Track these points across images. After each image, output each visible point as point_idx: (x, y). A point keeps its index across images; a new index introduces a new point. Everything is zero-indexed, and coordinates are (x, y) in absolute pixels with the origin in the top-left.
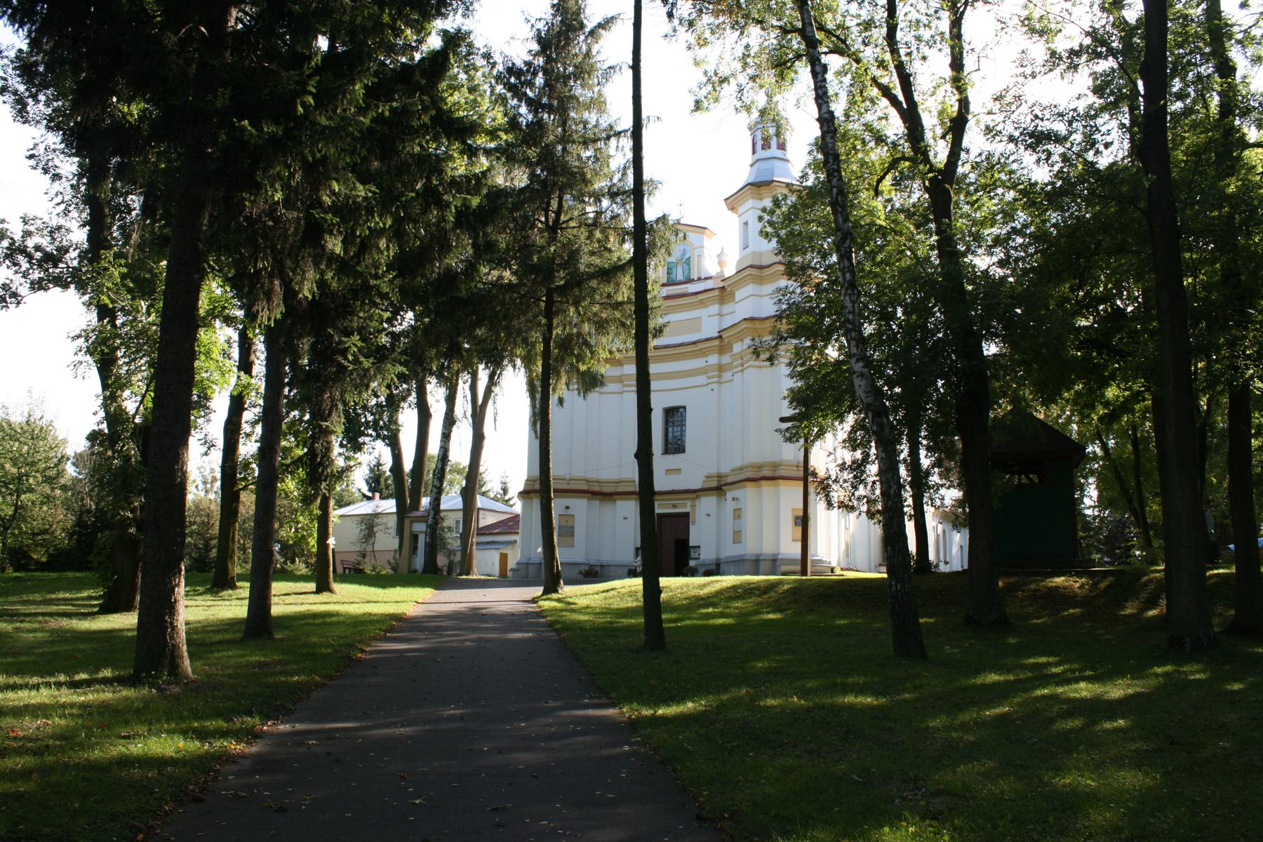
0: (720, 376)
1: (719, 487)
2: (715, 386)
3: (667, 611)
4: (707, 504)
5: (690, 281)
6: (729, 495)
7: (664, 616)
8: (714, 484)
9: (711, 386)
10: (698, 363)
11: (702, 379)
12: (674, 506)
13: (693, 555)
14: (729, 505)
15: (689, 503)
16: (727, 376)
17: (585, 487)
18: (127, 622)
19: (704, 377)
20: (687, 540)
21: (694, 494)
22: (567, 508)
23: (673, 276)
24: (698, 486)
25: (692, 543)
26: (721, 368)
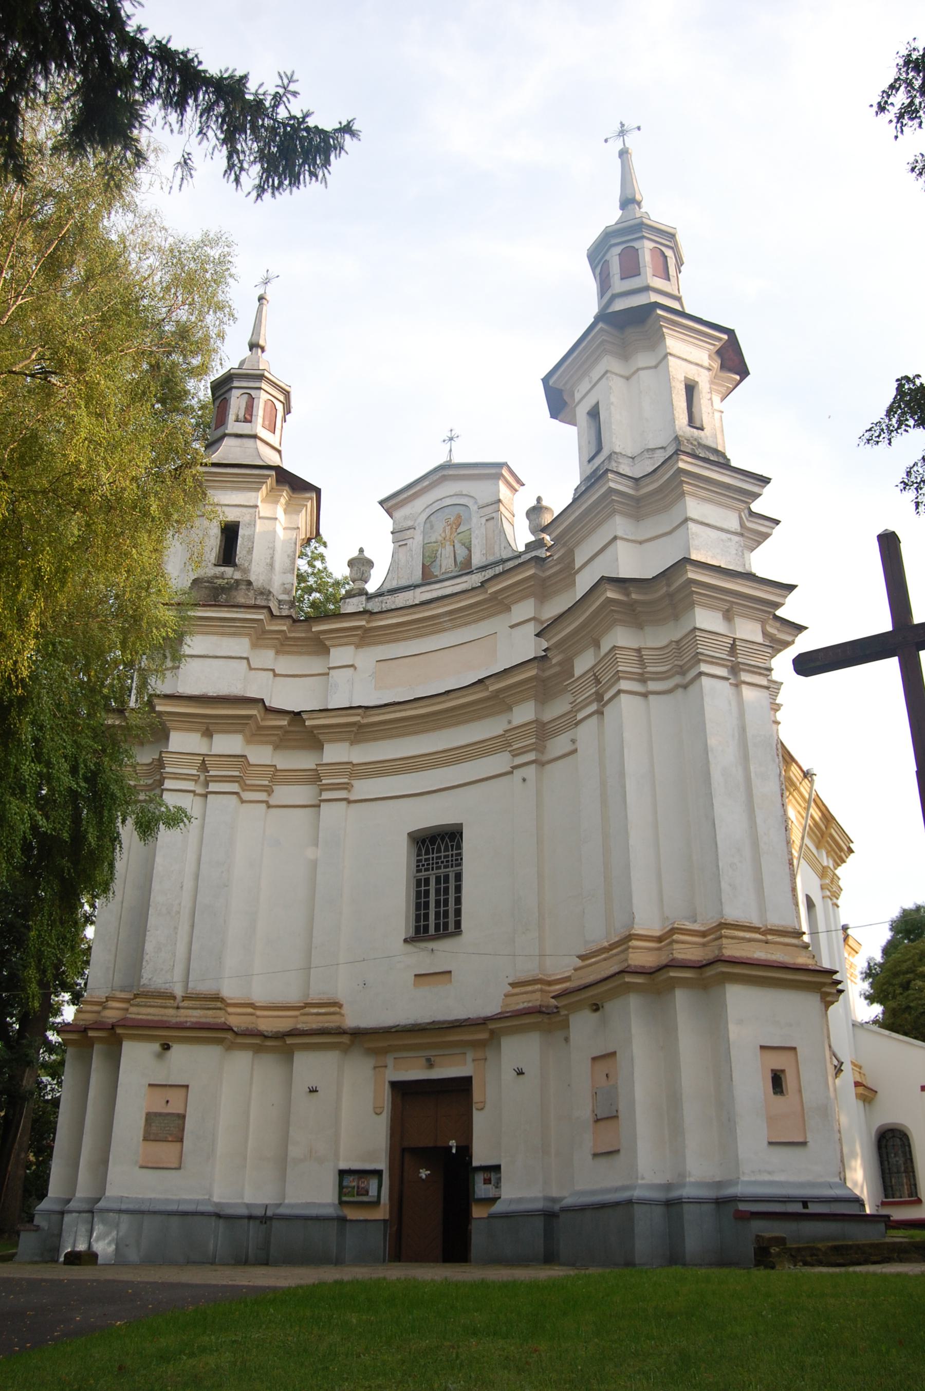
1: (546, 1011)
9: (519, 774)
11: (499, 762)
13: (481, 1189)
16: (559, 745)
21: (483, 1032)
24: (491, 1007)
26: (542, 732)
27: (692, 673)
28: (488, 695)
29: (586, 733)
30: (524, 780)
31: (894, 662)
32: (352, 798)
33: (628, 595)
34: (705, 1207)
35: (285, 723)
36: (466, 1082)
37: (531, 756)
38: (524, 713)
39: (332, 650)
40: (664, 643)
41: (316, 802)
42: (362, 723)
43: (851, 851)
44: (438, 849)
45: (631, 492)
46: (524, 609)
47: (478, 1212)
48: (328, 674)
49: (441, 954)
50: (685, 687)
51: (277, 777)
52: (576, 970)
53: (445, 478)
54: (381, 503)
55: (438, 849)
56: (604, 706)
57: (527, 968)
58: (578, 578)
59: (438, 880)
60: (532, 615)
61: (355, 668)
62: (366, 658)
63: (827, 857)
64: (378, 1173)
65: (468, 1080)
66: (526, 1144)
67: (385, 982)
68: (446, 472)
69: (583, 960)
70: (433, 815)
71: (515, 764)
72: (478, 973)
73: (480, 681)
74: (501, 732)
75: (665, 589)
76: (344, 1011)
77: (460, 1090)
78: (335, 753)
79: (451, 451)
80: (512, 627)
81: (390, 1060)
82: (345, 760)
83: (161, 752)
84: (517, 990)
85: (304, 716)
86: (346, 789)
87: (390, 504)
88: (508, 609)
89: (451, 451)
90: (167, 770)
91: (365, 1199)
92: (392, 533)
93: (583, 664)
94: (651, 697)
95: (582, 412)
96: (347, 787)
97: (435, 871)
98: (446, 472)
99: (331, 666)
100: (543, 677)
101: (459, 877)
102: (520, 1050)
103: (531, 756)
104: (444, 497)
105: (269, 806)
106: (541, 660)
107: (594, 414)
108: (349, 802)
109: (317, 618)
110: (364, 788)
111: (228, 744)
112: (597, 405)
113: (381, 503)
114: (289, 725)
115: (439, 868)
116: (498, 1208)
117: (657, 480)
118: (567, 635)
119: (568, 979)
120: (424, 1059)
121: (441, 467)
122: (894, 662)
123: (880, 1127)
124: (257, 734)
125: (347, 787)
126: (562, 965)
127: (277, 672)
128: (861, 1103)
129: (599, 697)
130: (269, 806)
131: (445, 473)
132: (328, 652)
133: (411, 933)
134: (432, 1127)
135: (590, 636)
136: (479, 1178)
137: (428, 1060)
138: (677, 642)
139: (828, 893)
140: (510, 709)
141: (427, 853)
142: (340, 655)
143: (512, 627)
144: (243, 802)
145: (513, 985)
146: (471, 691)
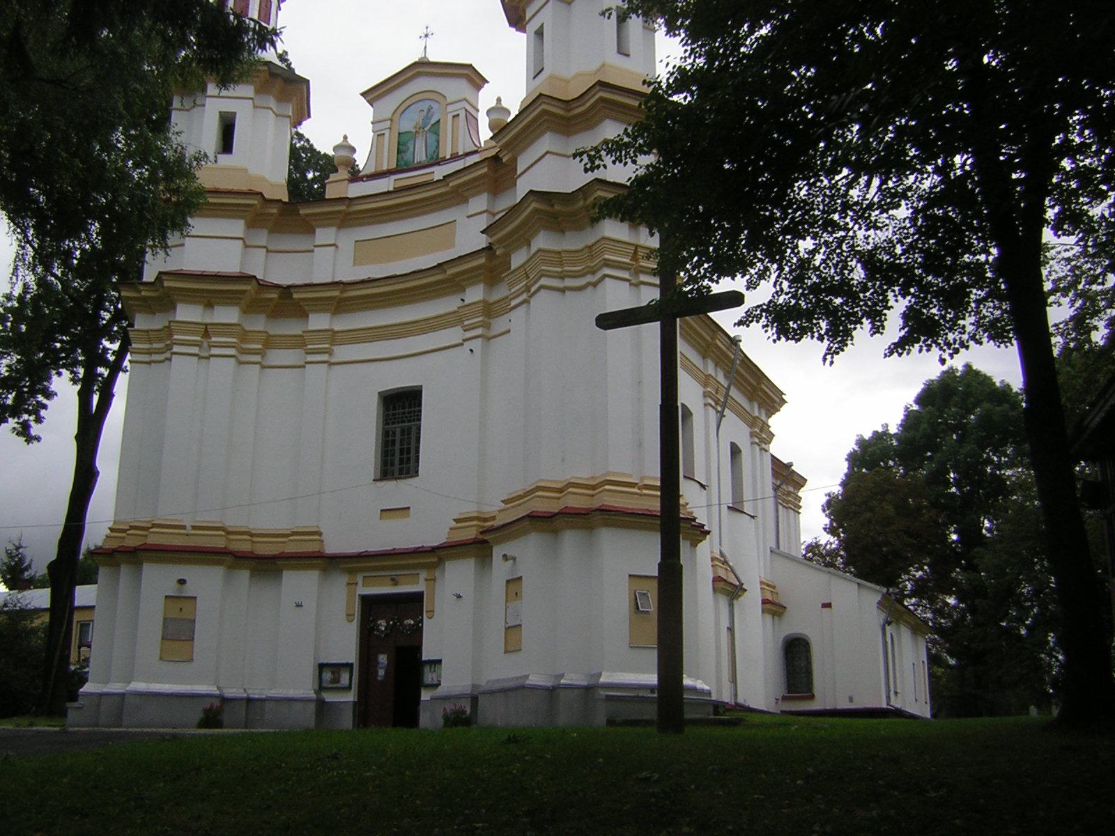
0: (487, 326)
1: (479, 543)
2: (477, 345)
3: (656, 496)
4: (458, 576)
5: (439, 162)
6: (498, 552)
7: (659, 493)
8: (470, 534)
9: (468, 345)
10: (447, 305)
11: (453, 335)
12: (395, 582)
13: (429, 677)
14: (500, 570)
15: (423, 575)
16: (499, 324)
17: (220, 543)
18: (726, 636)
19: (458, 329)
20: (418, 649)
21: (433, 557)
22: (182, 582)
23: (408, 156)
24: (437, 537)
25: (425, 656)
26: (490, 311)
27: (599, 275)
28: (444, 279)
29: (517, 316)
30: (471, 351)
31: (656, 325)
32: (333, 360)
33: (552, 206)
34: (576, 692)
35: (275, 296)
36: (417, 598)
37: (479, 331)
38: (475, 294)
39: (318, 230)
40: (579, 246)
41: (303, 363)
42: (342, 297)
43: (784, 402)
44: (401, 408)
45: (561, 112)
46: (479, 203)
47: (425, 696)
48: (313, 251)
49: (398, 491)
50: (595, 285)
51: (270, 342)
52: (499, 511)
53: (419, 74)
54: (363, 94)
55: (401, 408)
56: (530, 297)
57: (470, 509)
58: (519, 181)
59: (403, 431)
60: (485, 208)
61: (337, 247)
62: (348, 239)
63: (759, 408)
64: (350, 666)
65: (421, 594)
66: (462, 645)
67: (357, 513)
68: (420, 70)
69: (457, 522)
70: (398, 378)
71: (464, 338)
72: (434, 504)
73: (439, 265)
74: (456, 309)
75: (581, 203)
76: (323, 537)
77: (415, 600)
78: (319, 321)
79: (425, 47)
80: (468, 217)
81: (359, 579)
82: (327, 327)
83: (170, 322)
84: (459, 525)
85: (292, 290)
86: (327, 353)
87: (372, 95)
88: (466, 201)
89: (425, 47)
90: (175, 337)
91: (339, 685)
92: (372, 123)
93: (518, 259)
94: (567, 293)
95: (532, 27)
96: (329, 352)
97: (400, 425)
98: (420, 70)
99: (317, 243)
100: (490, 265)
101: (419, 429)
102: (458, 574)
103: (479, 331)
104: (421, 89)
105: (263, 367)
106: (489, 248)
107: (539, 33)
108: (331, 364)
109: (311, 189)
110: (343, 352)
111: (227, 315)
112: (542, 26)
113: (363, 94)
114: (280, 297)
115: (403, 422)
116: (440, 691)
117: (584, 104)
118: (506, 234)
119: (493, 518)
120: (389, 578)
121: (415, 65)
122: (656, 325)
123: (789, 635)
124: (252, 307)
125: (329, 352)
126: (493, 505)
127: (269, 248)
128: (768, 617)
129: (528, 289)
130: (263, 367)
131: (421, 68)
132: (314, 232)
133: (379, 477)
134: (392, 629)
135: (522, 237)
136: (427, 669)
137: (393, 580)
138: (590, 247)
139: (757, 440)
140: (464, 290)
141: (394, 408)
142: (324, 235)
143: (468, 217)
144: (241, 363)
145: (457, 521)
146: (436, 271)
